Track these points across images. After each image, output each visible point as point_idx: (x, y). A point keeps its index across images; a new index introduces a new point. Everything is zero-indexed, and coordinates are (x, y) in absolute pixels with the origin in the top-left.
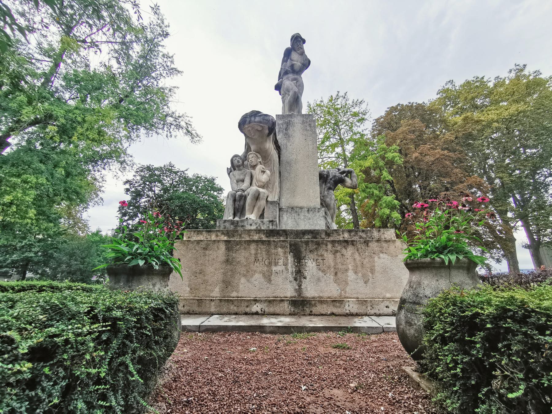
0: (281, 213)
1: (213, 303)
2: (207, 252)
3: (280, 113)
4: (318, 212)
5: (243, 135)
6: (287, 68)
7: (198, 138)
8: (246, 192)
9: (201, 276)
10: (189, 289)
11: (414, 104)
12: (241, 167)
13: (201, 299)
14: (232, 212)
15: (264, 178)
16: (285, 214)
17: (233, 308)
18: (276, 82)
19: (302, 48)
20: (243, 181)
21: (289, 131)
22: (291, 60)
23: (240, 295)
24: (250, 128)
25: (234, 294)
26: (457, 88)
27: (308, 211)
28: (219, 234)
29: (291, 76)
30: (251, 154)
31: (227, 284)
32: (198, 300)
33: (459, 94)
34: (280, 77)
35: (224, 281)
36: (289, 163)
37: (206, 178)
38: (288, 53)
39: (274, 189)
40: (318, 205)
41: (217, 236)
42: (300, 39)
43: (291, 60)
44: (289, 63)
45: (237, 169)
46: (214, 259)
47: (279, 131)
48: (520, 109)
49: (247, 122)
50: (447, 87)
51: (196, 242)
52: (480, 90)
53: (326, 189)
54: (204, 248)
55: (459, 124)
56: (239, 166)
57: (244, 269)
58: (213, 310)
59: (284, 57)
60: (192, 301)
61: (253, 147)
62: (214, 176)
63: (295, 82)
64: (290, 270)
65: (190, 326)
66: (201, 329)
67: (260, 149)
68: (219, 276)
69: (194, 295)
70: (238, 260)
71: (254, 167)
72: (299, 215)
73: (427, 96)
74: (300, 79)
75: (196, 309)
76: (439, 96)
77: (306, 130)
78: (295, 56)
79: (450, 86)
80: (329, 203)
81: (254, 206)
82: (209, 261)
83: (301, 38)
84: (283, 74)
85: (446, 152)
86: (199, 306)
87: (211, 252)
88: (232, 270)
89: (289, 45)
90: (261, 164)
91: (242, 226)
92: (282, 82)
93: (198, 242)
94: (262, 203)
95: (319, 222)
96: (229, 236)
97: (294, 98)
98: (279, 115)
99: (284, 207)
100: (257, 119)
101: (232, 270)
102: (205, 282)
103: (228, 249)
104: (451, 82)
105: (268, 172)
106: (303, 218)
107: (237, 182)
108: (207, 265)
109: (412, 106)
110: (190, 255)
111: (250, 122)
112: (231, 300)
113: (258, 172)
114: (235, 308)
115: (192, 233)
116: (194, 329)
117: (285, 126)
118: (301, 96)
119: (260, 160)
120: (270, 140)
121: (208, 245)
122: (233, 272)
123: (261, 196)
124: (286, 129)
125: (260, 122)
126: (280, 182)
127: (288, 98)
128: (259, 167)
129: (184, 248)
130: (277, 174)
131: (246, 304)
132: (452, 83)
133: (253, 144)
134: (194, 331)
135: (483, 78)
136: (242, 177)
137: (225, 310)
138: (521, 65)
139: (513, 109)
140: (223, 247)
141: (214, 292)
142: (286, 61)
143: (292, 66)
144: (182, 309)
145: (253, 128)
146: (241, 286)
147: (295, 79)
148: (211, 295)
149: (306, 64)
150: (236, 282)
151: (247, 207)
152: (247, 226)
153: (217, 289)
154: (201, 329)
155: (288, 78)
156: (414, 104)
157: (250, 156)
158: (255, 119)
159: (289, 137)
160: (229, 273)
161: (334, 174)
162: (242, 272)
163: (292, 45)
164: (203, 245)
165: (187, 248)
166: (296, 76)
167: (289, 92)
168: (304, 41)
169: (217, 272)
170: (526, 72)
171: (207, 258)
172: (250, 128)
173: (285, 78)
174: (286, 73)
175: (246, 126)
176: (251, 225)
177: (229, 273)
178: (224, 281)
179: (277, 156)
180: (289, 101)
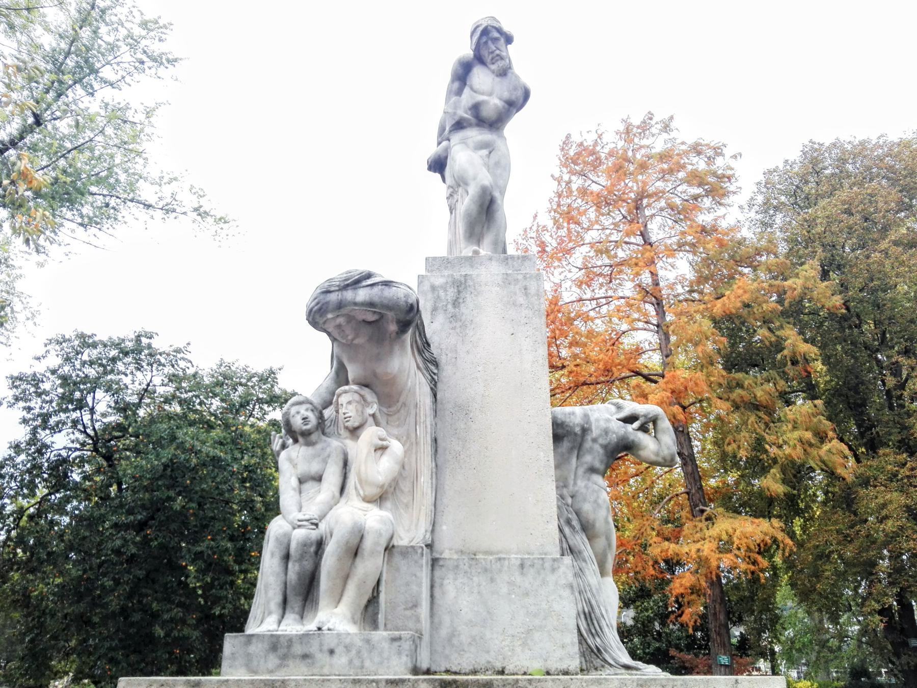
0: (438, 573)
3: (442, 251)
4: (553, 570)
5: (325, 335)
8: (322, 526)
12: (314, 437)
14: (279, 598)
15: (382, 469)
16: (451, 576)
20: (319, 479)
21: (463, 309)
22: (472, 89)
24: (341, 320)
27: (522, 566)
29: (475, 135)
30: (346, 392)
34: (443, 136)
36: (464, 410)
39: (418, 495)
40: (554, 550)
42: (496, 35)
43: (472, 89)
44: (467, 98)
45: (301, 439)
47: (435, 309)
53: (581, 471)
56: (306, 434)
59: (278, 499)
61: (353, 371)
63: (485, 152)
67: (375, 375)
71: (355, 432)
72: (492, 580)
74: (499, 143)
78: (481, 78)
80: (591, 517)
81: (346, 578)
83: (499, 30)
89: (467, 51)
90: (377, 424)
92: (447, 150)
94: (369, 566)
95: (556, 607)
97: (481, 206)
98: (434, 259)
99: (446, 555)
105: (396, 447)
106: (504, 590)
107: (301, 481)
113: (365, 451)
117: (451, 293)
118: (503, 193)
119: (374, 409)
120: (403, 347)
123: (368, 544)
124: (456, 303)
126: (437, 471)
127: (466, 202)
128: (371, 433)
130: (426, 448)
133: (351, 360)
136: (315, 468)
142: (459, 92)
147: (488, 146)
149: (516, 102)
155: (464, 142)
157: (343, 400)
159: (464, 326)
161: (603, 424)
163: (477, 49)
172: (341, 320)
173: (456, 137)
174: (459, 125)
179: (427, 389)
180: (468, 215)
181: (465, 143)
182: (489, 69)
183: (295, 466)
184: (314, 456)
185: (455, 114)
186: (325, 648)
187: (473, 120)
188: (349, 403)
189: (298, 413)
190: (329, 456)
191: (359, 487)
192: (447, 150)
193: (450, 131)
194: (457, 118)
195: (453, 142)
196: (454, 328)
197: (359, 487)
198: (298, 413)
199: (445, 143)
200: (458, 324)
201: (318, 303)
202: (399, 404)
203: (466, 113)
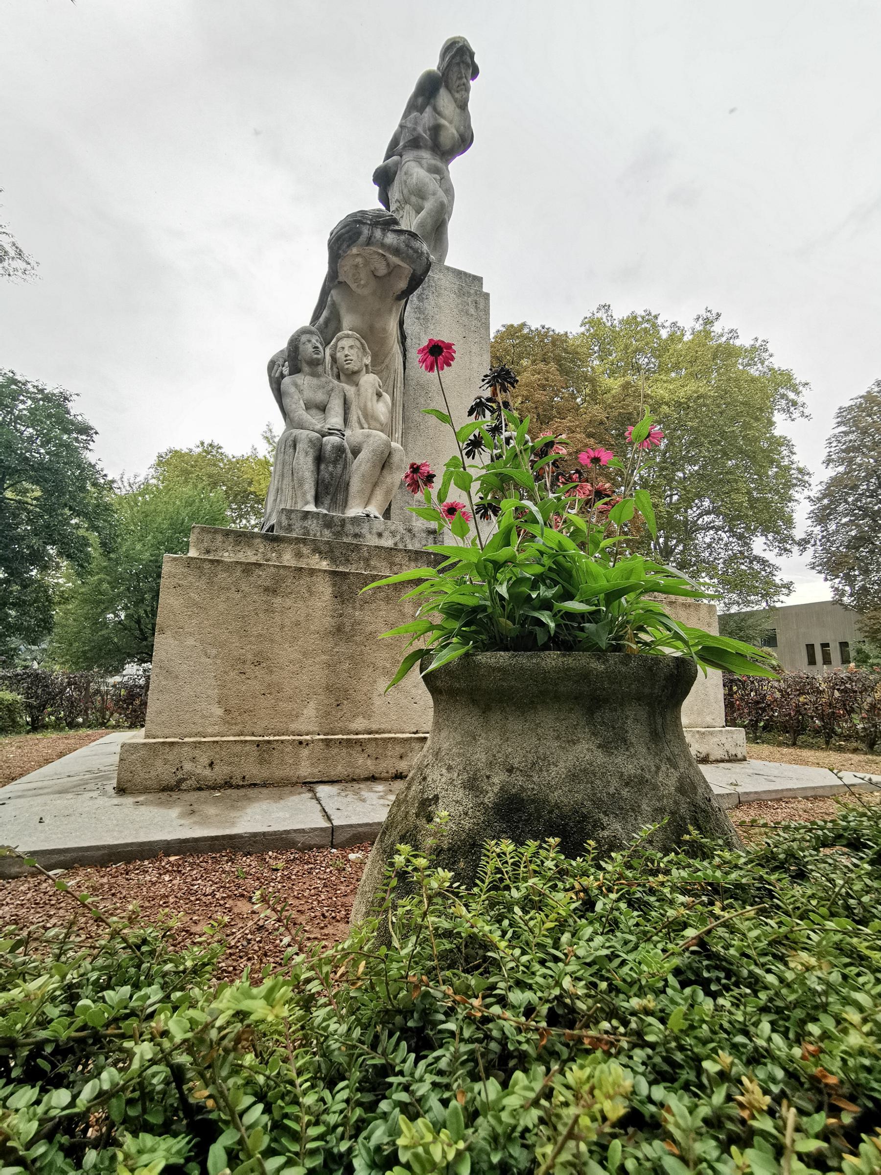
1: (305, 752)
2: (277, 601)
6: (420, 130)
7: (20, 264)
9: (259, 672)
10: (219, 712)
11: (551, 333)
13: (269, 742)
17: (364, 764)
18: (378, 160)
19: (467, 90)
22: (435, 109)
23: (374, 727)
24: (359, 260)
25: (359, 724)
26: (616, 322)
28: (305, 550)
29: (426, 155)
31: (339, 696)
32: (258, 744)
33: (615, 336)
35: (329, 689)
37: (41, 391)
38: (428, 90)
41: (299, 555)
43: (435, 109)
44: (427, 117)
45: (306, 368)
46: (298, 624)
48: (701, 390)
49: (363, 239)
50: (599, 315)
51: (239, 569)
52: (649, 338)
54: (267, 589)
55: (613, 392)
57: (384, 654)
58: (305, 770)
60: (238, 748)
62: (69, 388)
64: (821, 674)
65: (303, 831)
66: (340, 838)
68: (314, 673)
69: (237, 729)
70: (370, 628)
73: (568, 324)
75: (252, 770)
76: (583, 329)
77: (467, 313)
79: (601, 315)
81: (375, 485)
82: (282, 627)
84: (405, 143)
85: (592, 441)
86: (262, 761)
87: (289, 602)
88: (351, 657)
89: (433, 64)
91: (356, 536)
92: (397, 164)
93: (248, 568)
96: (333, 560)
100: (391, 239)
101: (351, 657)
102: (272, 689)
103: (339, 596)
104: (606, 307)
108: (277, 638)
109: (546, 335)
110: (222, 607)
111: (369, 242)
112: (357, 741)
114: (369, 762)
115: (219, 538)
116: (317, 841)
121: (278, 580)
122: (357, 661)
123: (396, 458)
125: (396, 252)
129: (202, 584)
131: (399, 750)
132: (607, 311)
133: (352, 310)
134: (320, 847)
135: (656, 317)
136: (320, 397)
137: (340, 770)
138: (714, 312)
139: (692, 387)
140: (325, 589)
141: (301, 719)
142: (421, 110)
143: (436, 130)
144: (207, 772)
145: (367, 263)
146: (377, 701)
148: (293, 727)
150: (365, 689)
151: (355, 485)
152: (368, 536)
153: (310, 711)
154: (340, 838)
155: (418, 160)
156: (551, 333)
158: (384, 235)
159: (426, 319)
160: (346, 666)
162: (380, 663)
164: (263, 577)
165: (211, 583)
166: (439, 164)
167: (423, 198)
168: (475, 72)
169: (310, 662)
170: (717, 328)
171: (277, 618)
173: (409, 156)
174: (415, 143)
175: (355, 251)
176: (380, 535)
177: (346, 666)
178: (329, 689)
181: (420, 163)
182: (453, 96)
183: (301, 391)
184: (320, 387)
185: (415, 129)
186: (375, 531)
187: (430, 143)
188: (351, 347)
189: (309, 341)
190: (332, 390)
191: (363, 421)
192: (397, 164)
193: (405, 147)
194: (415, 134)
195: (406, 158)
196: (418, 319)
197: (363, 421)
198: (309, 341)
199: (395, 158)
200: (422, 317)
201: (348, 232)
202: (384, 365)
203: (425, 132)
